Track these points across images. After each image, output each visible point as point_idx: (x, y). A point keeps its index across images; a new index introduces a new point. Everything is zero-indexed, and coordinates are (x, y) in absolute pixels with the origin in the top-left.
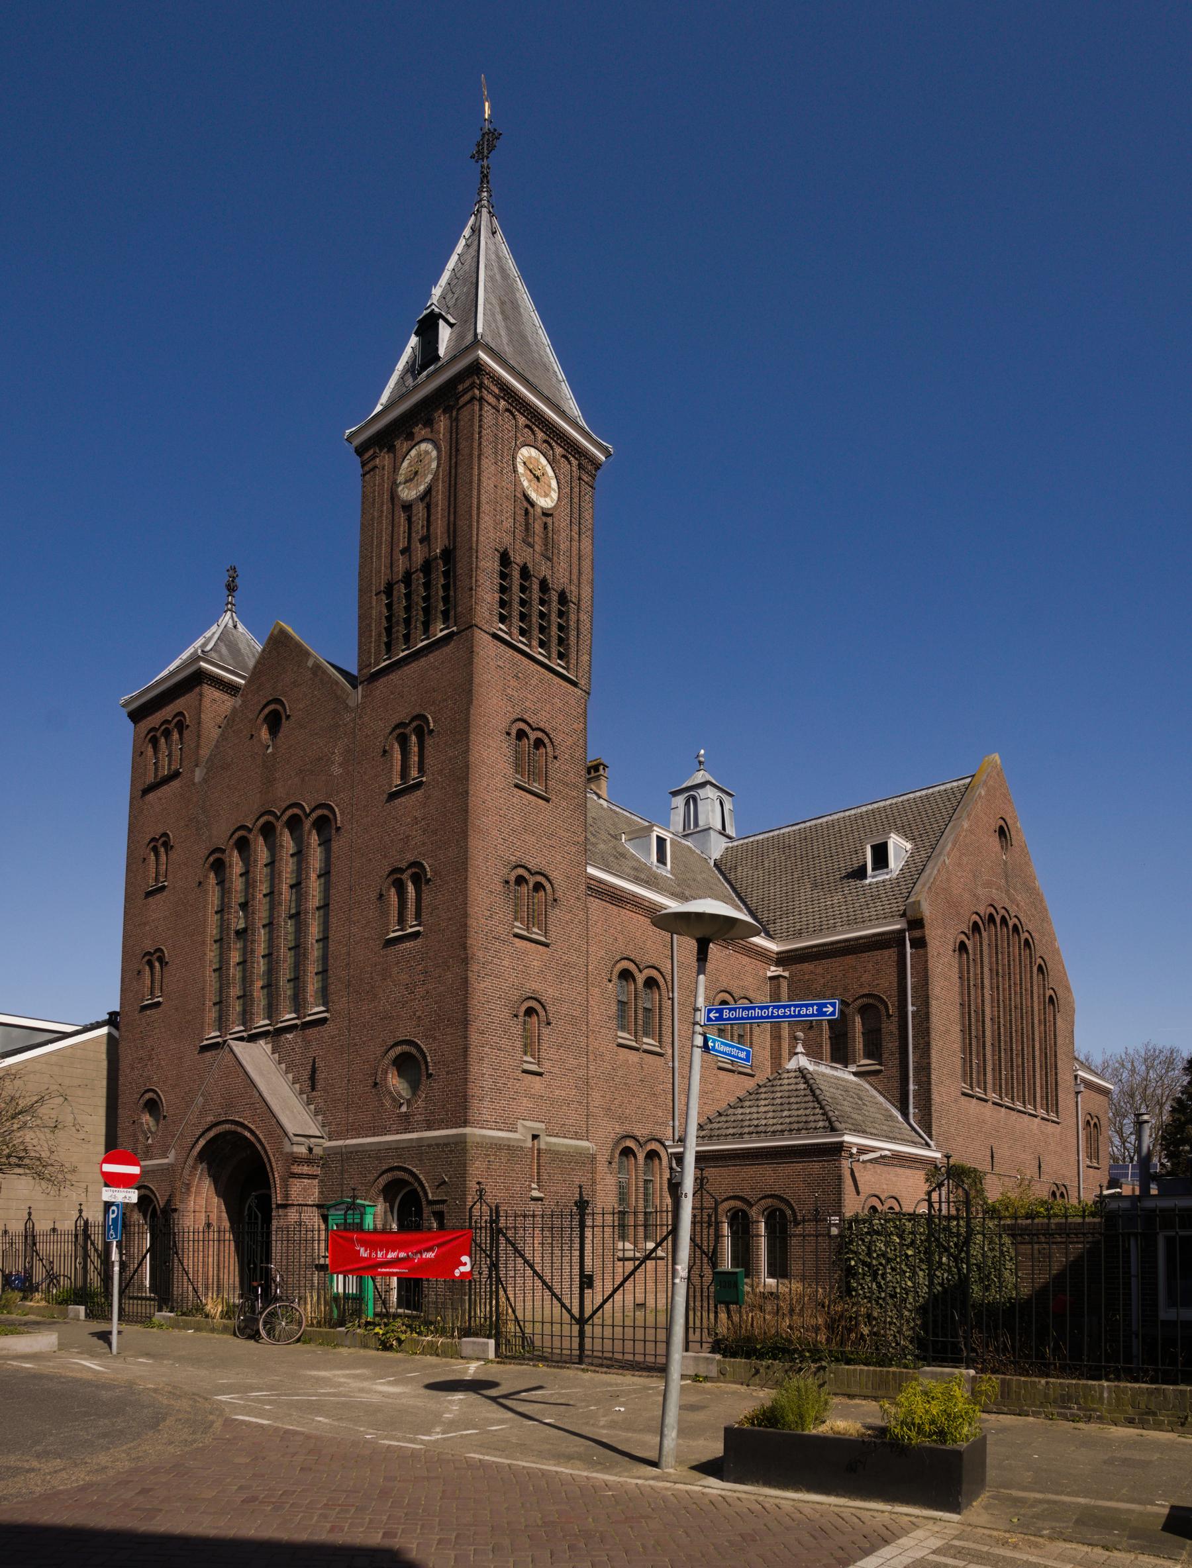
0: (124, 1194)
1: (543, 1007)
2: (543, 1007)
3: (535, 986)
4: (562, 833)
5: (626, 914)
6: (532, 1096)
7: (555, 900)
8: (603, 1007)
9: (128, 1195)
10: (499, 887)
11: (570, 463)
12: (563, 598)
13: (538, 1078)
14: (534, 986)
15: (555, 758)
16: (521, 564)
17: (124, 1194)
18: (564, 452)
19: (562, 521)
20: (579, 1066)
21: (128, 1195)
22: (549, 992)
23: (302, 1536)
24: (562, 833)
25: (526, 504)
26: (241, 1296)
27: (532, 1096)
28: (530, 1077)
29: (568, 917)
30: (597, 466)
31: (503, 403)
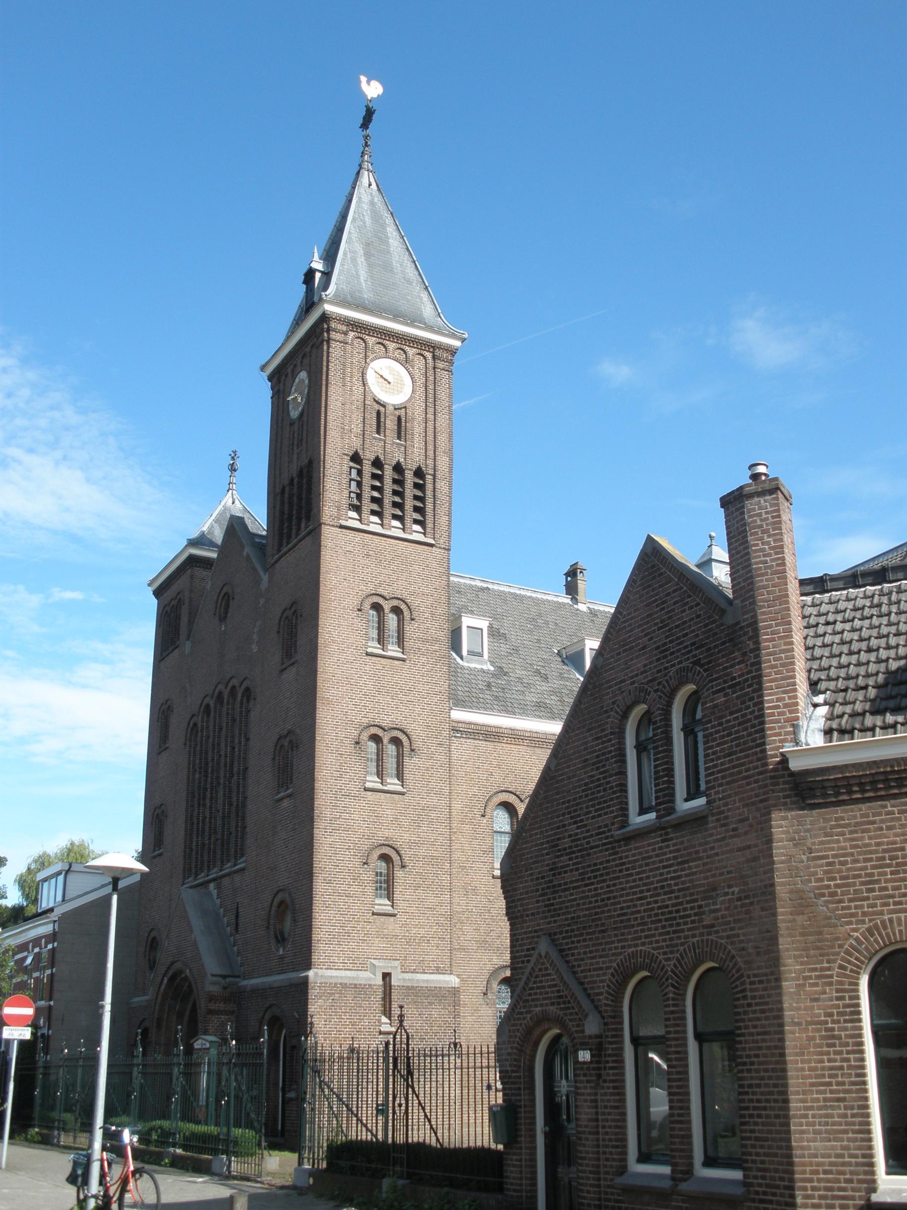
0: (19, 1032)
1: (398, 852)
2: (398, 852)
3: (387, 833)
4: (420, 687)
5: (503, 748)
6: (385, 936)
7: (412, 750)
8: (475, 842)
9: (23, 1032)
10: (349, 747)
11: (425, 358)
12: (419, 473)
13: (392, 919)
14: (385, 833)
15: (412, 619)
16: (372, 458)
17: (19, 1032)
18: (418, 351)
19: (417, 412)
20: (441, 904)
21: (23, 1032)
22: (402, 838)
23: (315, 915)
24: (420, 687)
25: (377, 407)
26: (143, 857)
27: (385, 936)
28: (382, 918)
29: (429, 764)
30: (453, 351)
31: (352, 334)
